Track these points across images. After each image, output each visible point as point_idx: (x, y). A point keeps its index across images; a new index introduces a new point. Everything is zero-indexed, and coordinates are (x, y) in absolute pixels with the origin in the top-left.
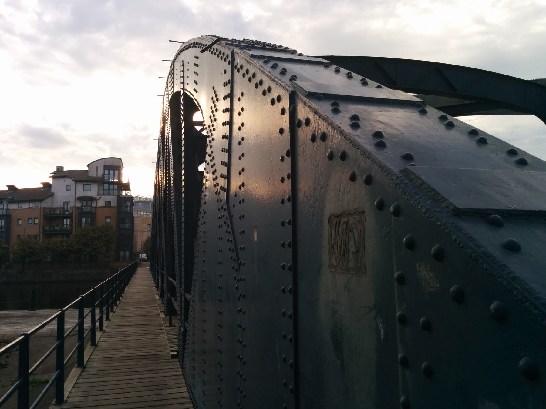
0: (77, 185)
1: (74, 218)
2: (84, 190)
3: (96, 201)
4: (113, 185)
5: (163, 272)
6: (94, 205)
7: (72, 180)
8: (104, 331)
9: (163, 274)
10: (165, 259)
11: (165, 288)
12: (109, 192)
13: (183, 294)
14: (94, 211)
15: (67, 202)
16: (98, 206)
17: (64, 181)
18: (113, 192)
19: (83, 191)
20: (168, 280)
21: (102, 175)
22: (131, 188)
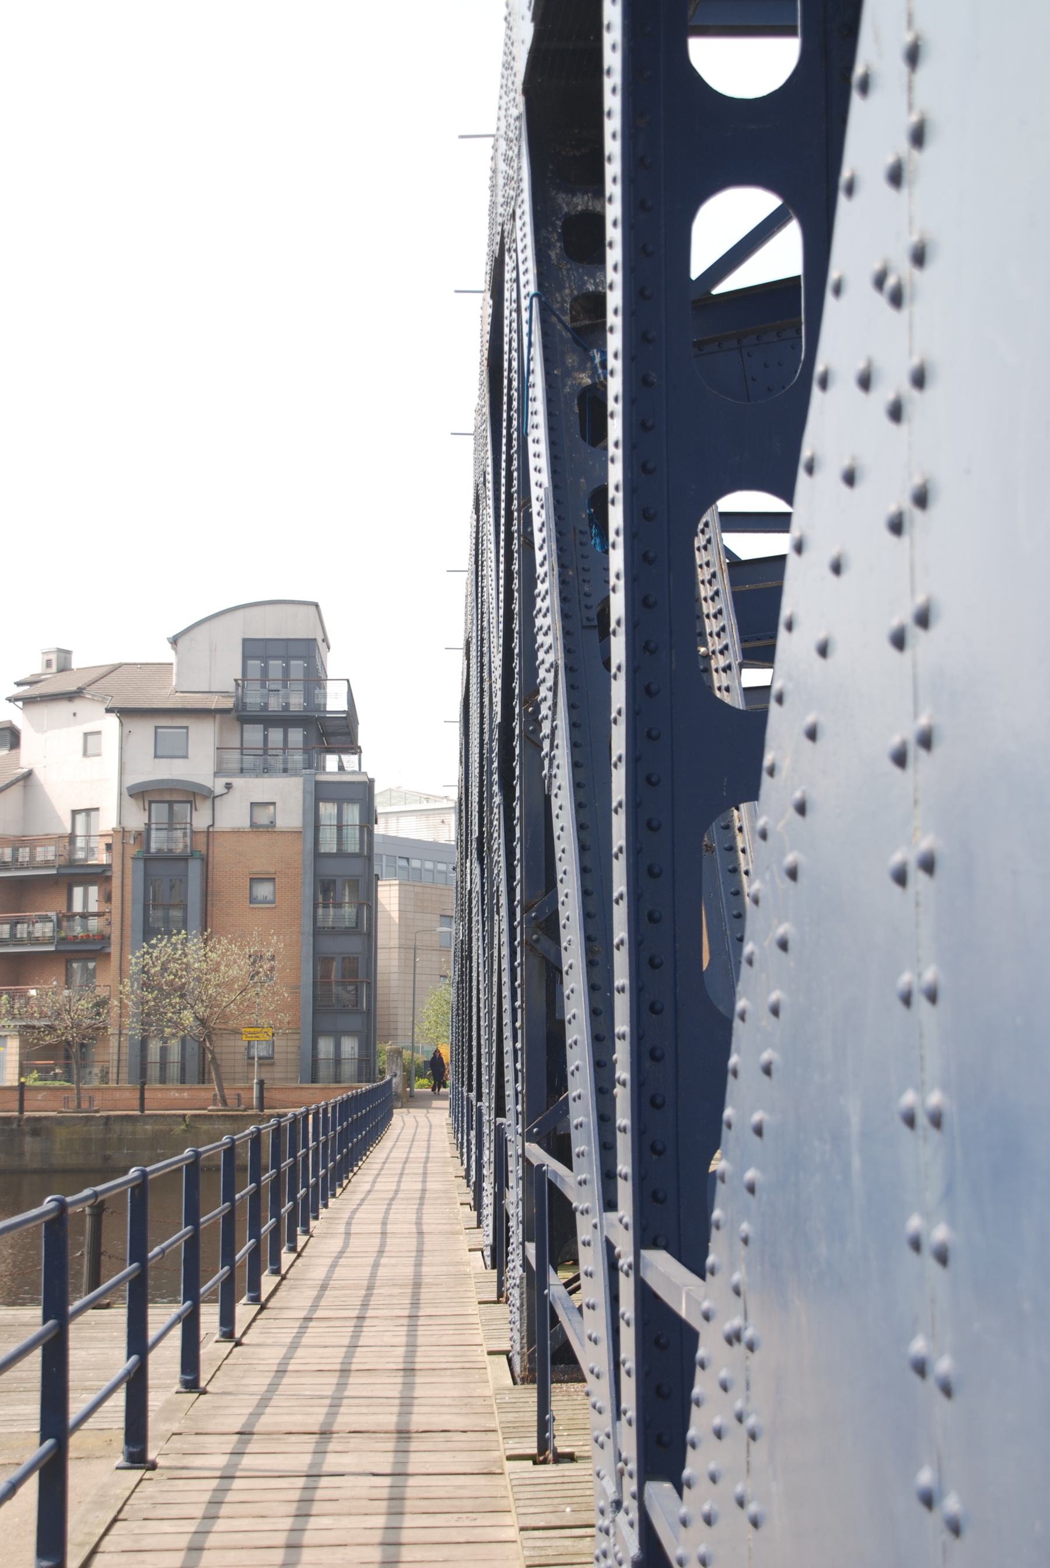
0: (126, 731)
1: (116, 882)
2: (159, 754)
3: (209, 802)
4: (281, 730)
5: (500, 1120)
6: (201, 820)
7: (109, 710)
8: (153, 1467)
9: (499, 1131)
10: (508, 1046)
11: (511, 1210)
12: (265, 761)
13: (631, 1259)
14: (202, 848)
15: (88, 811)
16: (217, 825)
17: (75, 714)
18: (285, 762)
19: (156, 757)
20: (527, 1163)
21: (234, 683)
22: (364, 737)
